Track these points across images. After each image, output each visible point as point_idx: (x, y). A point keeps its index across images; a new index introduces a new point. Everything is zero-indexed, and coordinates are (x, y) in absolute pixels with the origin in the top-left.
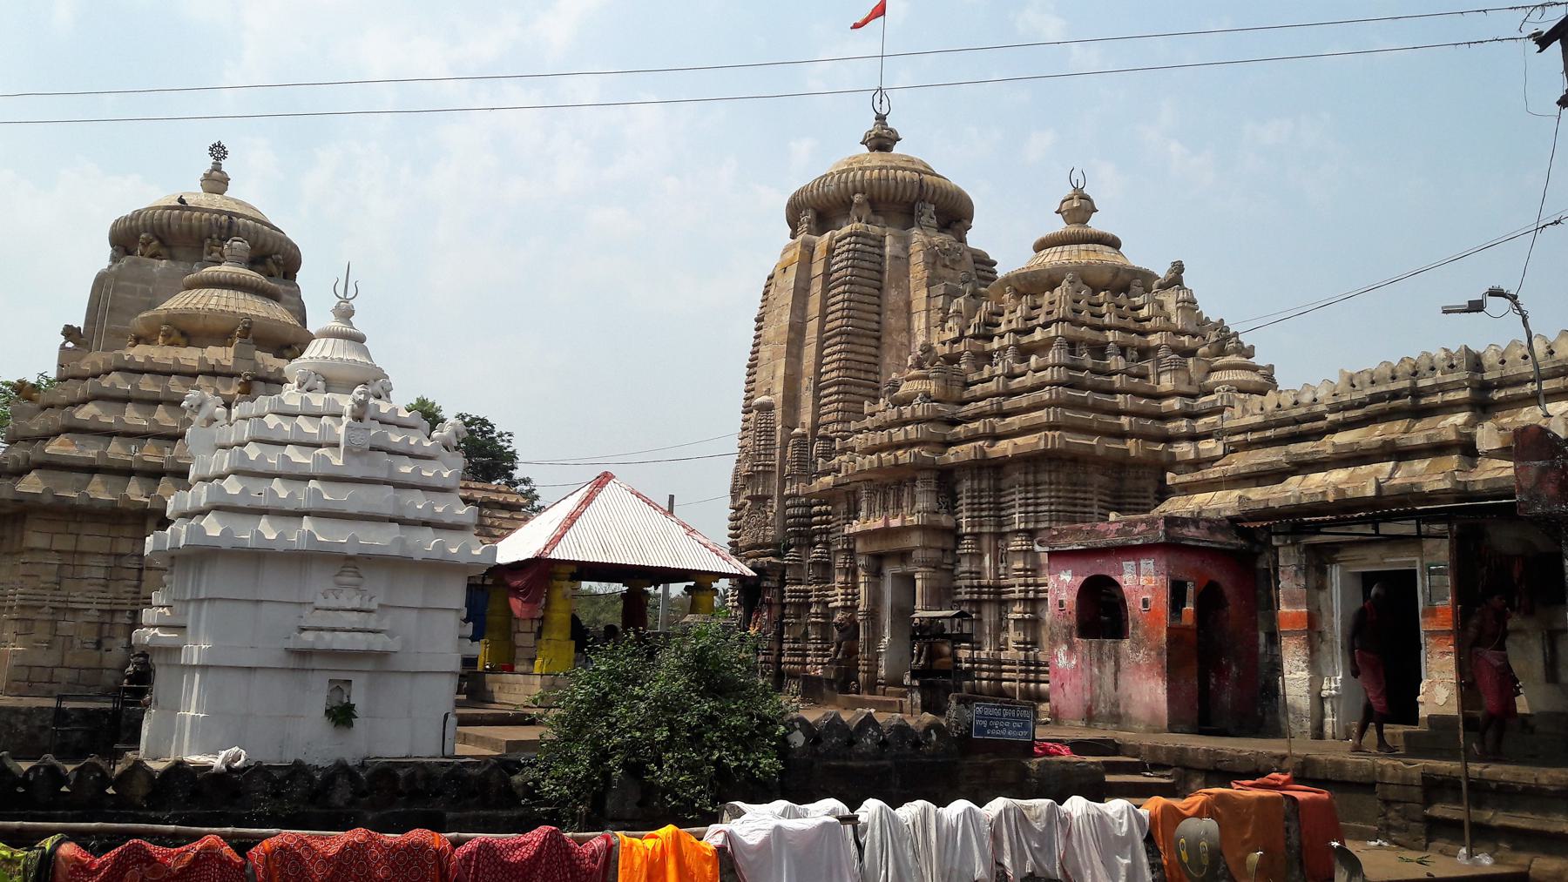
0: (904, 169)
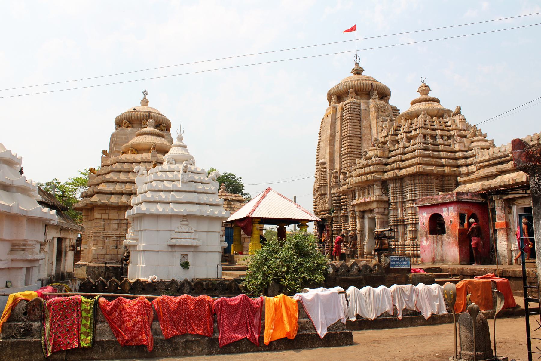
0: (366, 80)
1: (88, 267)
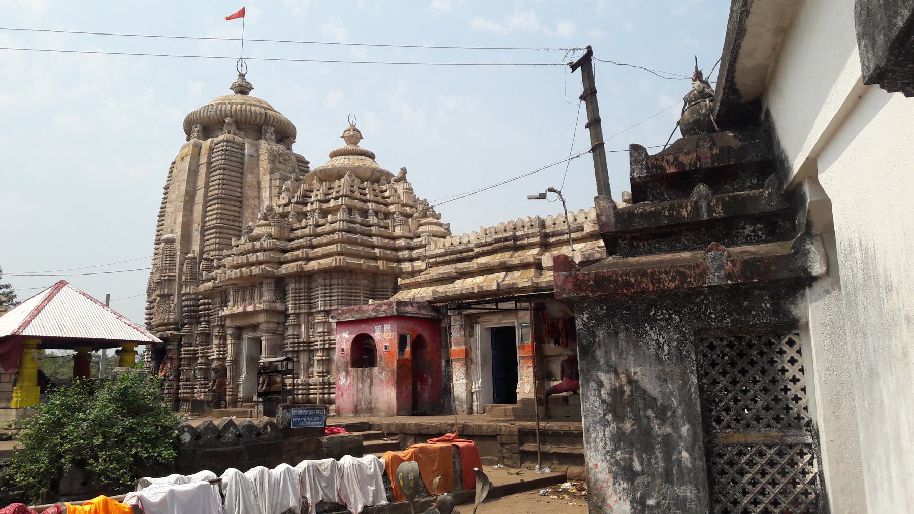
0: (256, 106)
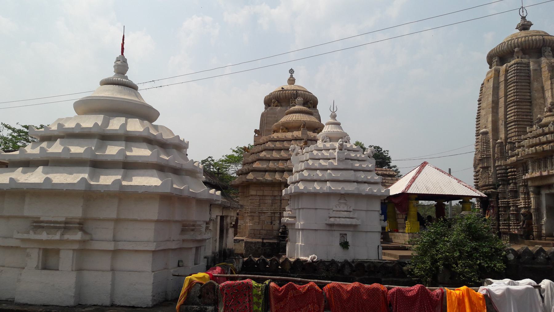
0: (535, 35)
1: (246, 243)
